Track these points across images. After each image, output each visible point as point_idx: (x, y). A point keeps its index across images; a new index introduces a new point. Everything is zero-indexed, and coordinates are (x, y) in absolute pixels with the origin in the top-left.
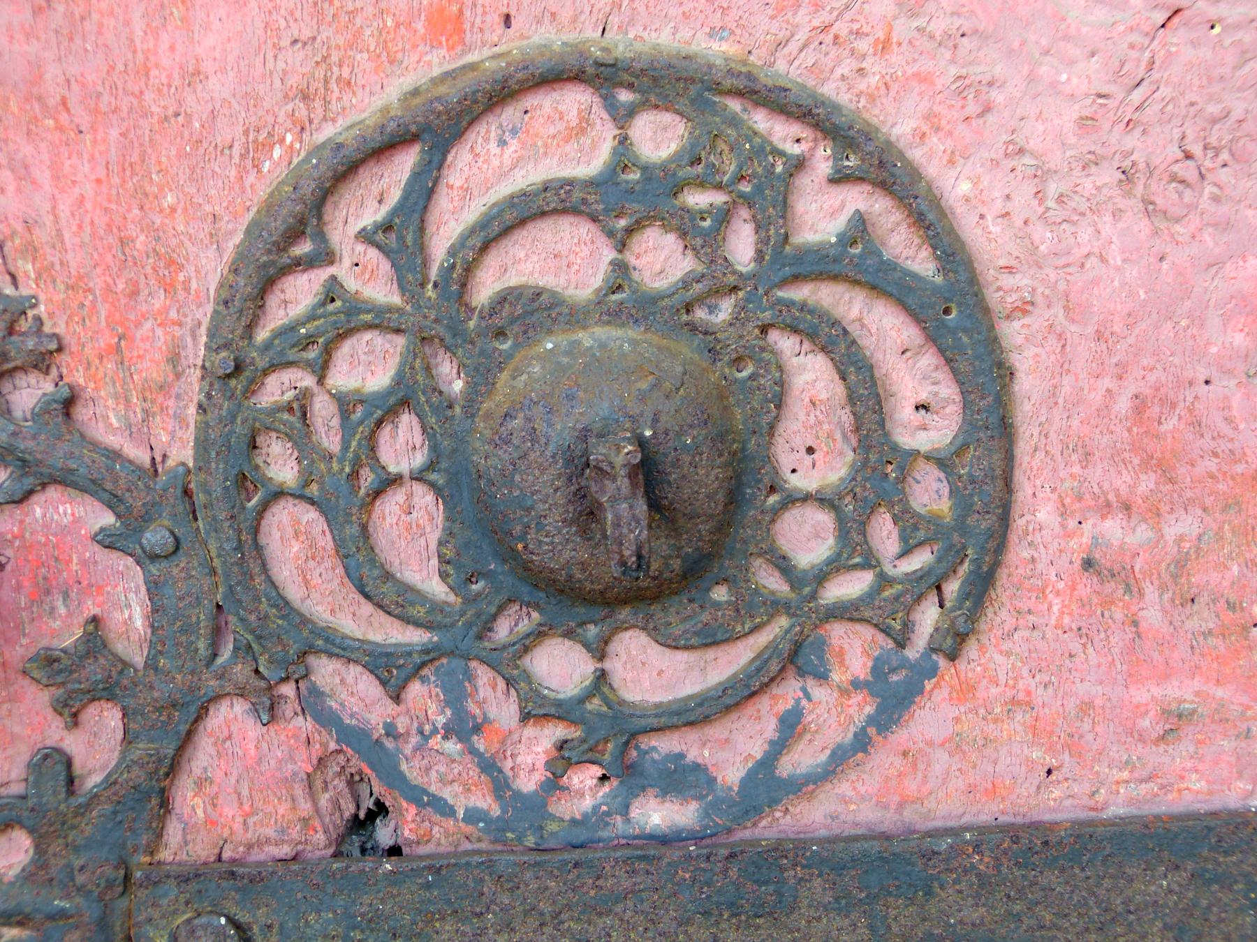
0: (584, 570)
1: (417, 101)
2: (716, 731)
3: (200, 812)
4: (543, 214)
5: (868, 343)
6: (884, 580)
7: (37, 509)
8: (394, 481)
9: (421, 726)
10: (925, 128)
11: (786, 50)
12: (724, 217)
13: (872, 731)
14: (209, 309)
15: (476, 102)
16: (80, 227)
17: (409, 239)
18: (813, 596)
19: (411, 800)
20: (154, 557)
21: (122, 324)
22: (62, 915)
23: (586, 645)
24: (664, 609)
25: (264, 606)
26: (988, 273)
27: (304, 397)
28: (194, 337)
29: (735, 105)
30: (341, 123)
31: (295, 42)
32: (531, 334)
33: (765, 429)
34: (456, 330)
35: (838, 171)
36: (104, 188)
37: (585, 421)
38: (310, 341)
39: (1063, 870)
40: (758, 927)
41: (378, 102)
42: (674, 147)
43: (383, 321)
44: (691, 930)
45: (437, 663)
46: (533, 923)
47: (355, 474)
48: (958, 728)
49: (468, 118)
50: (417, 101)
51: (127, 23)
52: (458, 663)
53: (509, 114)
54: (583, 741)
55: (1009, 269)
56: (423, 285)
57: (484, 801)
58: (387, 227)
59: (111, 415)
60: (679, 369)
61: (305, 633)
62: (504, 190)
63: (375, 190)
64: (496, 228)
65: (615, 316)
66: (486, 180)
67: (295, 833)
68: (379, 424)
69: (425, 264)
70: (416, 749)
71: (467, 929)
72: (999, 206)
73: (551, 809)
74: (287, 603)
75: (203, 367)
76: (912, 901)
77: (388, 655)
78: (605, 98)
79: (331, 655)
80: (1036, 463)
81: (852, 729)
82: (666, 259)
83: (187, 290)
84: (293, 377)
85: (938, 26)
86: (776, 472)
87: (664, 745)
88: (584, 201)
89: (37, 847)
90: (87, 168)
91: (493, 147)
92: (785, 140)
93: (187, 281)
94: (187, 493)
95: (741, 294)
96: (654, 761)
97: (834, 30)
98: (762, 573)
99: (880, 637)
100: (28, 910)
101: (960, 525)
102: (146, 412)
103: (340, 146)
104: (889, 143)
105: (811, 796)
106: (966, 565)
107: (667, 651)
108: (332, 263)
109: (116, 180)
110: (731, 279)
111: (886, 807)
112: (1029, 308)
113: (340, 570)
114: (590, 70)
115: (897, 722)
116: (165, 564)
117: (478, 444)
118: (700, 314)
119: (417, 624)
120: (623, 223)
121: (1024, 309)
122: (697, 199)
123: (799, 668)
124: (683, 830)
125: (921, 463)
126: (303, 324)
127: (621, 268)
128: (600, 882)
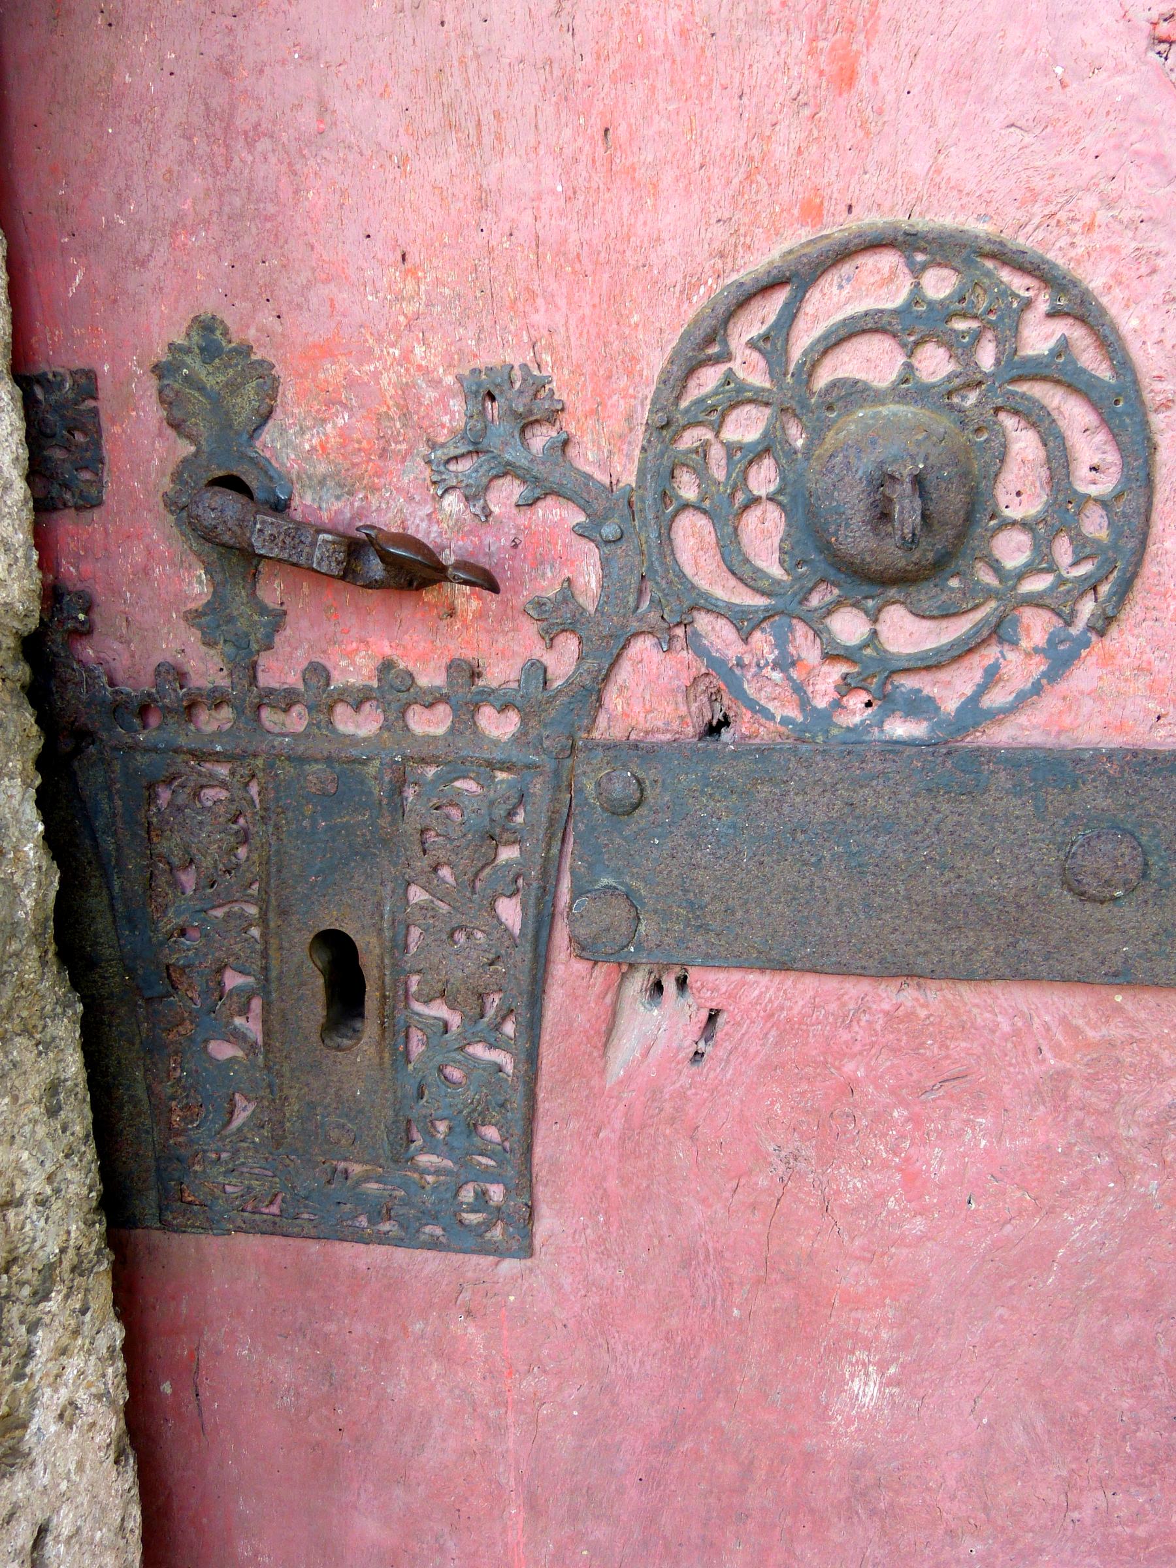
0: (872, 555)
1: (791, 257)
2: (943, 675)
3: (619, 708)
4: (864, 332)
5: (1062, 424)
6: (1061, 581)
7: (540, 510)
8: (757, 500)
9: (758, 660)
10: (1112, 283)
11: (1025, 230)
12: (977, 337)
13: (1044, 681)
14: (653, 388)
15: (828, 257)
16: (581, 334)
17: (779, 345)
18: (1014, 588)
19: (748, 708)
20: (607, 542)
21: (600, 396)
22: (535, 766)
23: (866, 613)
24: (918, 591)
25: (671, 575)
26: (1145, 381)
27: (706, 445)
28: (642, 405)
29: (989, 264)
30: (743, 272)
31: (719, 221)
32: (849, 407)
33: (993, 475)
34: (804, 404)
35: (1053, 308)
36: (597, 310)
37: (882, 457)
38: (713, 409)
39: (1165, 778)
40: (962, 802)
41: (766, 260)
42: (948, 291)
43: (758, 399)
44: (919, 800)
45: (772, 620)
46: (818, 789)
47: (732, 496)
48: (1100, 684)
49: (821, 269)
50: (791, 257)
51: (620, 207)
52: (785, 620)
53: (846, 268)
54: (859, 674)
55: (1160, 378)
56: (785, 374)
57: (793, 713)
58: (766, 338)
59: (589, 453)
60: (942, 430)
61: (694, 595)
62: (839, 317)
63: (760, 315)
64: (833, 339)
65: (903, 398)
66: (829, 311)
67: (675, 726)
68: (751, 462)
69: (787, 363)
70: (754, 676)
71: (777, 791)
72: (1156, 336)
73: (834, 720)
74: (684, 575)
75: (647, 424)
76: (1063, 790)
77: (743, 612)
78: (907, 258)
79: (708, 611)
80: (1167, 508)
81: (1031, 680)
82: (938, 364)
83: (641, 376)
84: (700, 433)
85: (1125, 216)
86: (997, 505)
87: (908, 683)
88: (890, 323)
89: (522, 720)
90: (588, 297)
91: (835, 290)
92: (1019, 288)
93: (641, 371)
94: (630, 504)
95: (983, 387)
96: (902, 693)
97: (1057, 217)
98: (981, 573)
99: (1055, 619)
100: (514, 760)
101: (1115, 546)
102: (610, 452)
103: (742, 284)
104: (1087, 289)
105: (1000, 723)
106: (1116, 572)
107: (917, 619)
108: (730, 360)
109: (605, 306)
110: (979, 377)
111: (1049, 734)
112: (1170, 404)
113: (718, 557)
114: (900, 239)
115: (1061, 676)
116: (613, 546)
117: (811, 476)
118: (956, 400)
119: (763, 593)
120: (912, 339)
121: (1166, 406)
122: (960, 325)
123: (1000, 637)
124: (916, 739)
125: (1091, 504)
126: (710, 397)
127: (909, 366)
128: (864, 765)
